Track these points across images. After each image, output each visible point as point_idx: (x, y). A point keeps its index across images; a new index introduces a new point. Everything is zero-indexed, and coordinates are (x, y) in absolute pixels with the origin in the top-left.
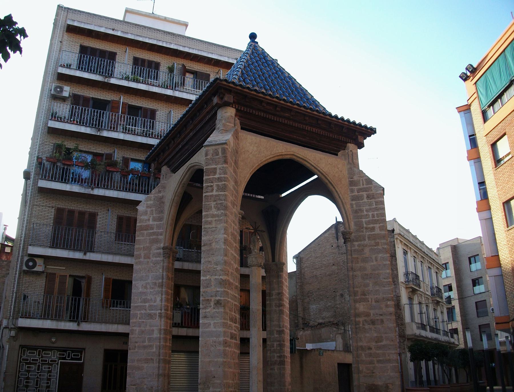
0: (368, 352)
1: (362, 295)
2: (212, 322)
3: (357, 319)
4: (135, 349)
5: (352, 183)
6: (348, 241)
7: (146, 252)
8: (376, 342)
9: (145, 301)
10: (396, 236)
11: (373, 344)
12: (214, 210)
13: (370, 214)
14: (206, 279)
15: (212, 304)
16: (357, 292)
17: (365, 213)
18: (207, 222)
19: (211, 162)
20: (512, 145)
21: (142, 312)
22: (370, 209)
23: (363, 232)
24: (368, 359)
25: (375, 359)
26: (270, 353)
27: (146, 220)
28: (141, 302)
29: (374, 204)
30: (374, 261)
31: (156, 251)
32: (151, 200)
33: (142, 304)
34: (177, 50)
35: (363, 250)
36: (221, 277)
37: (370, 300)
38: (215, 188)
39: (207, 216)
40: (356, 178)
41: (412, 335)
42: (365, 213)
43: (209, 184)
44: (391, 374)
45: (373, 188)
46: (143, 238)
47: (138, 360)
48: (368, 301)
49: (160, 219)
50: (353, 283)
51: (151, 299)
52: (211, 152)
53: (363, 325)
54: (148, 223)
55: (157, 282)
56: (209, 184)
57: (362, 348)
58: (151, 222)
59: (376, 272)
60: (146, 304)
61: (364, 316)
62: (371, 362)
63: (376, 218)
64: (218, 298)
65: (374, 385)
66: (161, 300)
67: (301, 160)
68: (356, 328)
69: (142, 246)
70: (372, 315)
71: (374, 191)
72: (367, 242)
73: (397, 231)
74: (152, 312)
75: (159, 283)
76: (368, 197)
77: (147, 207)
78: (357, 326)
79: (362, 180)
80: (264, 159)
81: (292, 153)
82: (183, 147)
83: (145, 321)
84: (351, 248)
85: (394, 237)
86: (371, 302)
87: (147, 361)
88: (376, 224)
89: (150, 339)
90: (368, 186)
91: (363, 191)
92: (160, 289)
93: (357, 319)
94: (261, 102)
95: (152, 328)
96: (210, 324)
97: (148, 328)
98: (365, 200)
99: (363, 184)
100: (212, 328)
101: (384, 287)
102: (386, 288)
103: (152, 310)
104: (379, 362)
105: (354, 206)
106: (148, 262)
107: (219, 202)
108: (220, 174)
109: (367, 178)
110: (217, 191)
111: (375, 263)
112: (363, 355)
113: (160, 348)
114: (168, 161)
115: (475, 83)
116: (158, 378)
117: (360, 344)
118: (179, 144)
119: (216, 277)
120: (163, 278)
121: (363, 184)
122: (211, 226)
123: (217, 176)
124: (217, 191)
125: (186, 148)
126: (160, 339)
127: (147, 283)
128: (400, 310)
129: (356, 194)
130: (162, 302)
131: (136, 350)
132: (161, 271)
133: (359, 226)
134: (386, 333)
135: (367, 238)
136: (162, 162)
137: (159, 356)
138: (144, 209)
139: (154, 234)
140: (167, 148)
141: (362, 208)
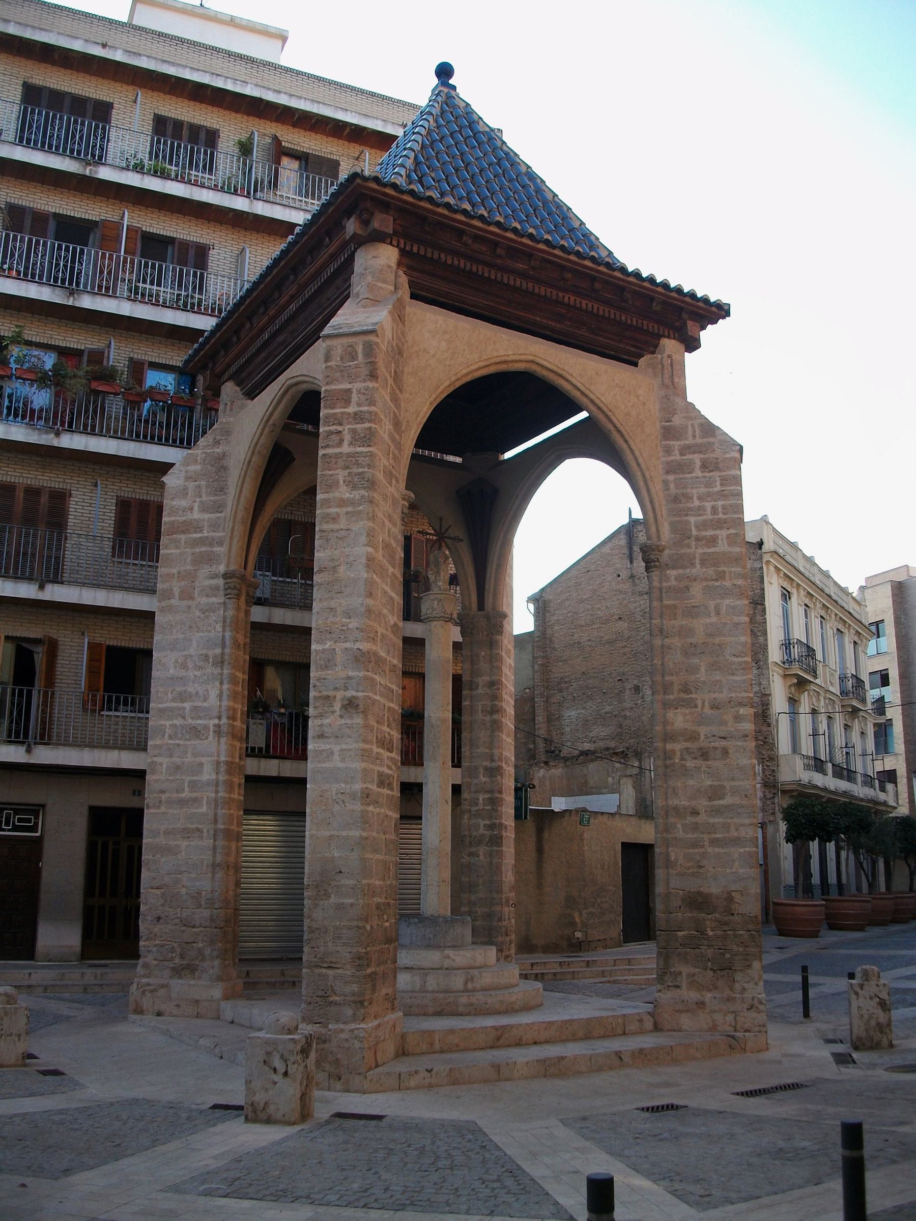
0: (690, 819)
3: (669, 746)
4: (159, 807)
6: (655, 566)
8: (710, 799)
9: (183, 697)
10: (766, 558)
13: (708, 505)
15: (337, 706)
16: (672, 683)
17: (697, 503)
19: (338, 374)
21: (175, 722)
22: (709, 495)
23: (689, 546)
24: (690, 836)
25: (706, 837)
26: (469, 819)
28: (174, 700)
29: (718, 483)
30: (713, 614)
31: (207, 583)
33: (175, 704)
35: (687, 588)
36: (358, 645)
38: (347, 437)
40: (677, 421)
43: (333, 428)
44: (741, 871)
46: (177, 551)
47: (167, 833)
48: (696, 707)
49: (218, 507)
50: (663, 664)
54: (189, 516)
56: (333, 428)
58: (196, 515)
59: (717, 640)
61: (685, 741)
63: (721, 516)
64: (350, 693)
65: (700, 894)
66: (220, 696)
68: (666, 767)
69: (175, 571)
70: (702, 737)
71: (718, 453)
72: (697, 570)
74: (199, 722)
75: (215, 656)
76: (704, 466)
77: (187, 478)
78: (668, 762)
79: (693, 425)
81: (531, 358)
82: (273, 336)
84: (661, 583)
87: (187, 833)
88: (721, 528)
89: (193, 785)
90: (705, 440)
91: (694, 453)
93: (669, 746)
95: (198, 759)
96: (332, 753)
97: (189, 759)
98: (698, 473)
99: (694, 436)
101: (733, 674)
104: (714, 842)
105: (672, 486)
106: (189, 607)
108: (359, 405)
109: (703, 421)
111: (714, 619)
112: (679, 826)
113: (216, 805)
116: (214, 873)
117: (674, 802)
119: (348, 645)
121: (694, 436)
123: (351, 409)
124: (351, 444)
125: (280, 339)
127: (186, 657)
128: (769, 725)
130: (221, 700)
132: (219, 628)
134: (733, 779)
137: (216, 822)
139: (202, 541)
141: (689, 491)
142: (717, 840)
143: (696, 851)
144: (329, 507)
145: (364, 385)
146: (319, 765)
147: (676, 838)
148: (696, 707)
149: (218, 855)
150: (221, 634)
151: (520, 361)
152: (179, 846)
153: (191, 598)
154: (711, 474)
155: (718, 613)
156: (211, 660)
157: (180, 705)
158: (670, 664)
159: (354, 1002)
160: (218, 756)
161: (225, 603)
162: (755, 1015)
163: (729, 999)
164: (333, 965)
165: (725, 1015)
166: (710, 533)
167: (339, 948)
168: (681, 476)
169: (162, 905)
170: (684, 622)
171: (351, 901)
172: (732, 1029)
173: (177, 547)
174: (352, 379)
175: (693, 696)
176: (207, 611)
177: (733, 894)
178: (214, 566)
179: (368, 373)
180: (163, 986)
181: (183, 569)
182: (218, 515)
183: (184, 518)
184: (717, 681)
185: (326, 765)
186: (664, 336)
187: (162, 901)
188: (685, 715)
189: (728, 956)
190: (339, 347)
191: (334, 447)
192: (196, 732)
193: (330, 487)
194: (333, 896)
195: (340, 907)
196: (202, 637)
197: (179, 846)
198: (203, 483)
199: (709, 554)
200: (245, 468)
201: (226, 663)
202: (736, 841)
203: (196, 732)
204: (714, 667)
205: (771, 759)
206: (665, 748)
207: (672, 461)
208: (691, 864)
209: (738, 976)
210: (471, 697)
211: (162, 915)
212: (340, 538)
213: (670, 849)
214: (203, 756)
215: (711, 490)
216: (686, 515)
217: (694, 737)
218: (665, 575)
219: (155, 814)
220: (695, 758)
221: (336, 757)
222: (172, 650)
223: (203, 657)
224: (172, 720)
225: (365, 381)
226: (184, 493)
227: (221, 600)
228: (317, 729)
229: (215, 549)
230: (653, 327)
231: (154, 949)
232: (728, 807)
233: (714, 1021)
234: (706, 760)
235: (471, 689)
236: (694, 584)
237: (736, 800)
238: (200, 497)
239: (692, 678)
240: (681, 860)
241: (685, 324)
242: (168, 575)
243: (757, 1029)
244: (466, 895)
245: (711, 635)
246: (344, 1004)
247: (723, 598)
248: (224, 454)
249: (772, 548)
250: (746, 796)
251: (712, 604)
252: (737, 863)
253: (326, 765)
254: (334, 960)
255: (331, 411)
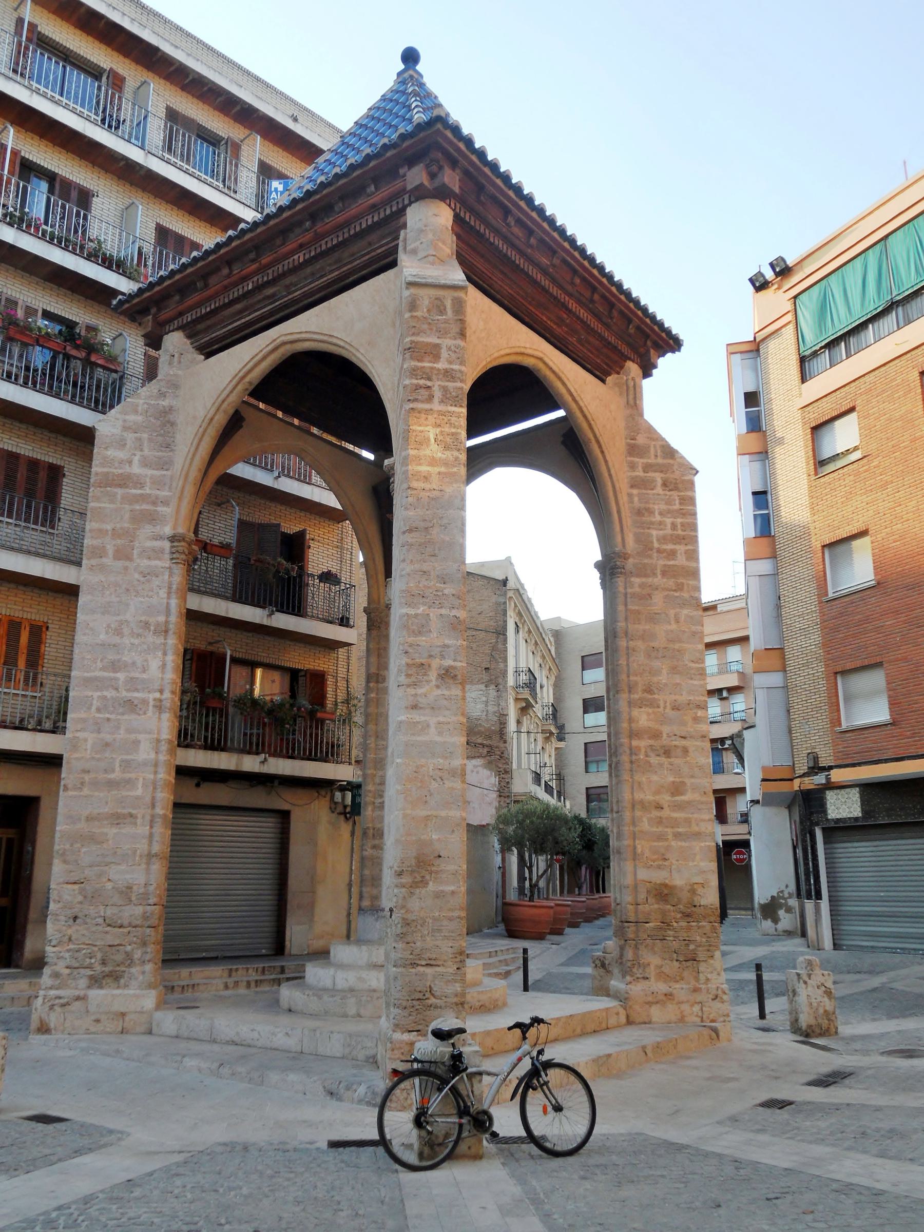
0: (655, 813)
1: (645, 691)
2: (433, 721)
3: (635, 743)
4: (81, 789)
5: (633, 450)
6: (621, 573)
7: (119, 541)
8: (673, 795)
9: (115, 666)
10: (510, 594)
11: (665, 798)
12: (434, 446)
13: (669, 521)
14: (416, 615)
15: (433, 675)
16: (636, 683)
17: (658, 518)
18: (418, 476)
19: (425, 326)
20: (866, 431)
21: (105, 693)
22: (669, 512)
23: (650, 557)
24: (655, 829)
25: (669, 830)
26: (373, 811)
27: (121, 462)
28: (103, 669)
29: (677, 502)
30: (673, 622)
31: (149, 544)
32: (136, 412)
33: (106, 674)
34: (156, 50)
35: (650, 595)
36: (454, 612)
37: (662, 704)
38: (438, 394)
39: (418, 460)
40: (641, 440)
41: (525, 794)
42: (658, 518)
43: (422, 382)
44: (702, 864)
45: (675, 467)
46: (112, 506)
47: (89, 819)
48: (659, 707)
49: (164, 465)
50: (628, 665)
51: (134, 663)
52: (426, 302)
53: (647, 756)
54: (127, 469)
55: (152, 620)
56: (422, 382)
57: (643, 805)
58: (136, 469)
59: (677, 646)
60: (118, 675)
61: (650, 738)
62: (660, 837)
63: (680, 532)
64: (448, 662)
65: (666, 886)
66: (164, 666)
67: (551, 377)
68: (631, 762)
69: (109, 527)
70: (665, 736)
71: (677, 475)
72: (658, 580)
73: (511, 584)
74: (136, 695)
75: (158, 624)
76: (665, 485)
77: (125, 428)
78: (634, 757)
79: (655, 446)
80: (496, 355)
81: (541, 355)
82: (259, 288)
83: (112, 717)
84: (626, 588)
85: (505, 594)
86: (665, 708)
87: (118, 819)
88: (680, 543)
89: (126, 765)
90: (666, 461)
91: (655, 471)
92: (160, 640)
93: (635, 743)
94: (507, 212)
95: (133, 736)
96: (428, 726)
97: (121, 735)
98: (659, 490)
99: (656, 456)
100: (433, 735)
101: (692, 679)
102: (695, 682)
103: (137, 690)
104: (677, 836)
105: (636, 499)
106: (126, 568)
107: (447, 429)
108: (450, 363)
109: (664, 443)
110: (442, 402)
111: (674, 626)
112: (645, 820)
113: (155, 788)
114: (193, 321)
115: (795, 297)
116: (148, 864)
117: (639, 796)
118: (245, 279)
119: (443, 611)
120: (168, 612)
121: (656, 456)
122: (427, 486)
123: (441, 365)
124: (442, 402)
125: (269, 291)
126: (156, 765)
127: (121, 623)
128: (505, 742)
129: (641, 474)
130: (163, 672)
131: (86, 791)
132: (163, 593)
133: (646, 546)
134: (692, 777)
135: (659, 572)
136: (170, 321)
137: (153, 806)
138: (117, 431)
139: (143, 498)
140: (199, 285)
141: (651, 506)
142: (680, 834)
143: (660, 844)
144: (420, 464)
145: (454, 342)
146: (414, 738)
147: (641, 832)
148: (659, 707)
149: (154, 843)
150: (165, 601)
151: (532, 356)
152: (107, 834)
153: (129, 558)
154: (672, 493)
155: (677, 621)
156: (152, 628)
157: (112, 675)
158: (635, 664)
159: (457, 1004)
160: (158, 733)
161: (170, 568)
162: (719, 1005)
163: (696, 990)
164: (432, 962)
165: (692, 1006)
166: (670, 547)
167: (437, 943)
168: (644, 491)
169: (81, 903)
170: (647, 627)
171: (452, 888)
172: (699, 1019)
173: (112, 502)
174: (442, 333)
175: (656, 696)
176: (147, 574)
177: (695, 886)
178: (158, 527)
179: (458, 330)
180: (78, 998)
181: (118, 526)
182: (165, 472)
183: (120, 471)
184: (678, 684)
185: (419, 738)
186: (630, 359)
187: (80, 898)
188: (648, 714)
189: (692, 947)
190: (425, 297)
191: (423, 402)
192: (131, 706)
193: (421, 444)
194: (431, 883)
195: (438, 895)
196: (142, 602)
197: (107, 834)
198: (145, 436)
199: (669, 566)
200: (204, 425)
201: (171, 632)
202: (698, 835)
203: (131, 706)
204: (674, 670)
205: (506, 772)
206: (631, 744)
207: (637, 476)
208: (656, 857)
209: (702, 967)
210: (378, 689)
211: (80, 915)
212: (433, 499)
213: (637, 842)
214: (140, 733)
215: (670, 507)
216: (649, 528)
217: (656, 735)
218: (630, 582)
219: (75, 797)
220: (658, 755)
221: (432, 730)
222: (103, 614)
223: (143, 624)
224: (102, 691)
225: (455, 339)
226: (121, 444)
227: (167, 564)
228: (411, 698)
229: (159, 509)
230: (625, 350)
231: (67, 955)
232: (689, 803)
233: (682, 1012)
234: (669, 757)
235: (377, 682)
236: (656, 592)
237: (696, 796)
238: (142, 450)
239: (655, 679)
240: (647, 853)
241: (648, 351)
242: (100, 530)
243: (722, 1019)
244: (368, 889)
245: (669, 641)
246: (446, 1007)
247: (681, 607)
248: (171, 409)
249: (514, 587)
250: (705, 793)
251: (672, 613)
252: (698, 857)
253: (419, 738)
254: (434, 956)
255: (420, 364)
